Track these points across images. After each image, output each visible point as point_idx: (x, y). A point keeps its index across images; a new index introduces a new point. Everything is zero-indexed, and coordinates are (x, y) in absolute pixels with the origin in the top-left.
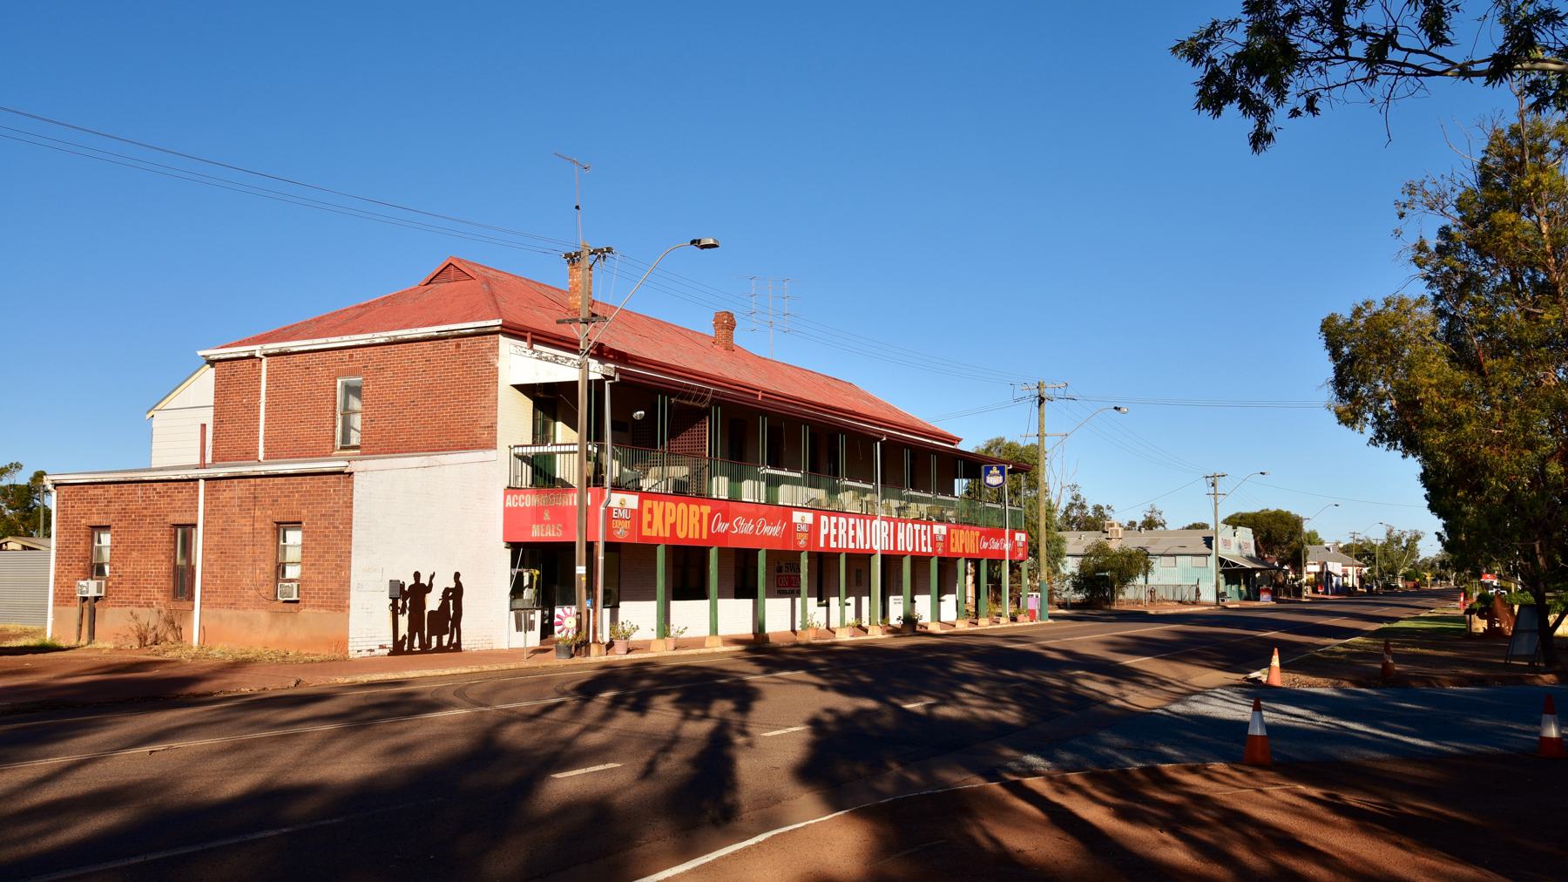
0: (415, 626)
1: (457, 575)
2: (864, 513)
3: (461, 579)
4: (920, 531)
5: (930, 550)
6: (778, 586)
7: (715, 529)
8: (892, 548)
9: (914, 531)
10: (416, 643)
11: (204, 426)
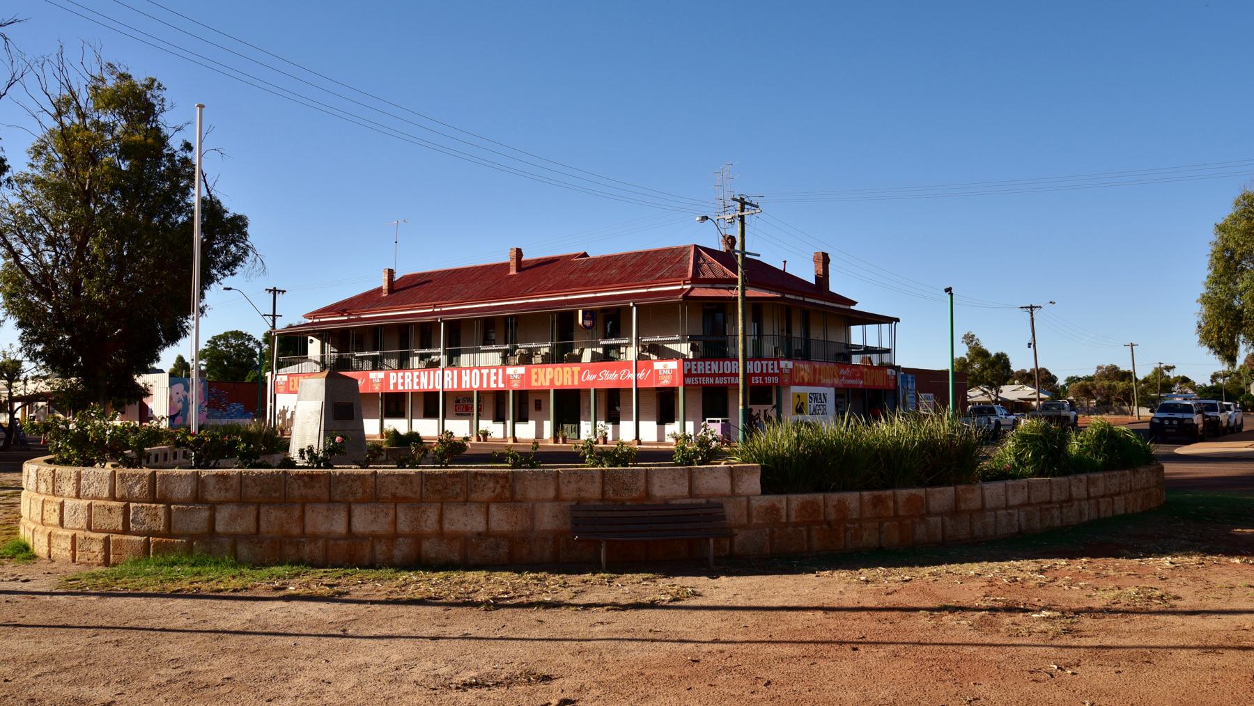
2: (472, 366)
6: (456, 411)
7: (585, 378)
8: (455, 387)
11: (759, 255)
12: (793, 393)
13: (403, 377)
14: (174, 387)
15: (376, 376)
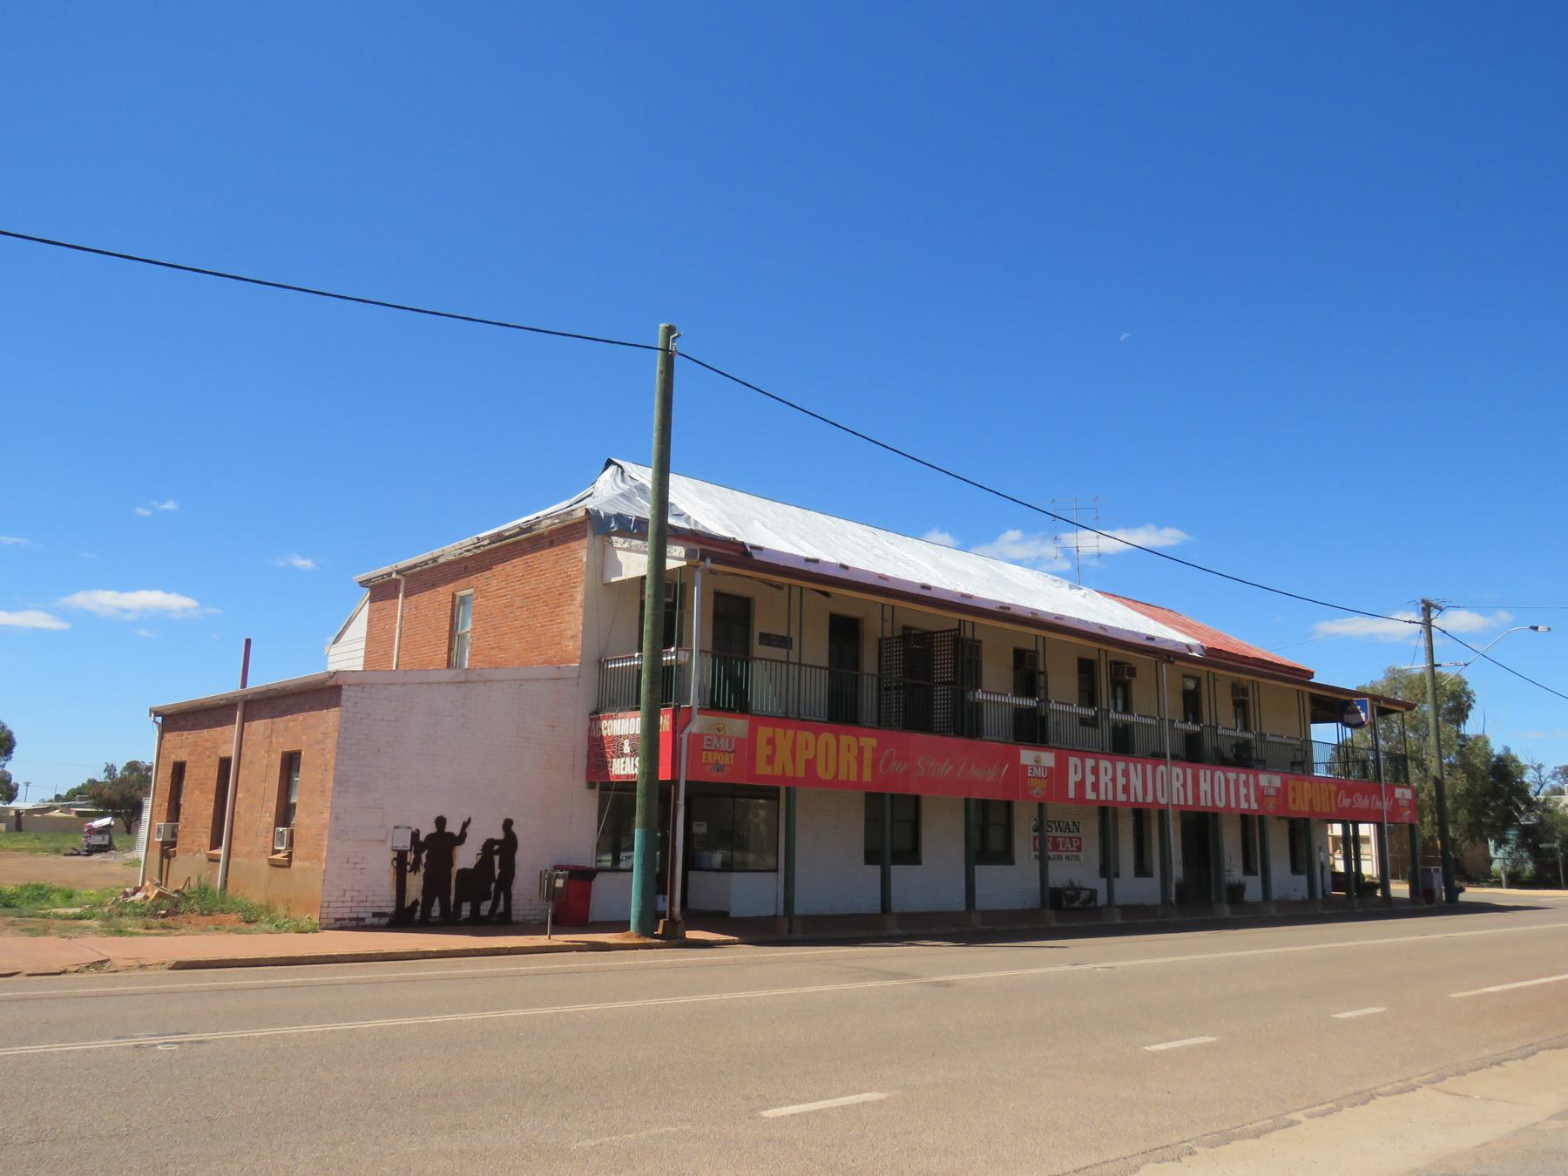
0: (430, 890)
1: (508, 824)
3: (514, 828)
4: (1237, 782)
5: (1254, 806)
8: (1190, 802)
10: (436, 911)
13: (1095, 771)
14: (167, 736)
15: (1037, 760)
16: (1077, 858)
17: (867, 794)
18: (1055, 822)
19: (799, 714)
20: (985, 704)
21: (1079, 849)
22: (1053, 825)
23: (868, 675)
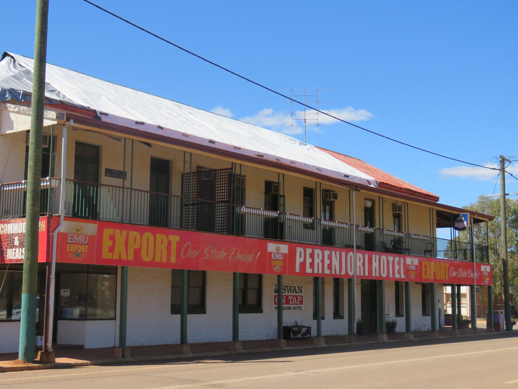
4: (393, 262)
5: (403, 276)
8: (367, 274)
9: (388, 262)
12: (403, 316)
13: (312, 256)
16: (300, 308)
17: (361, 280)
18: (287, 286)
19: (130, 221)
20: (247, 215)
21: (301, 302)
22: (286, 289)
23: (174, 196)
